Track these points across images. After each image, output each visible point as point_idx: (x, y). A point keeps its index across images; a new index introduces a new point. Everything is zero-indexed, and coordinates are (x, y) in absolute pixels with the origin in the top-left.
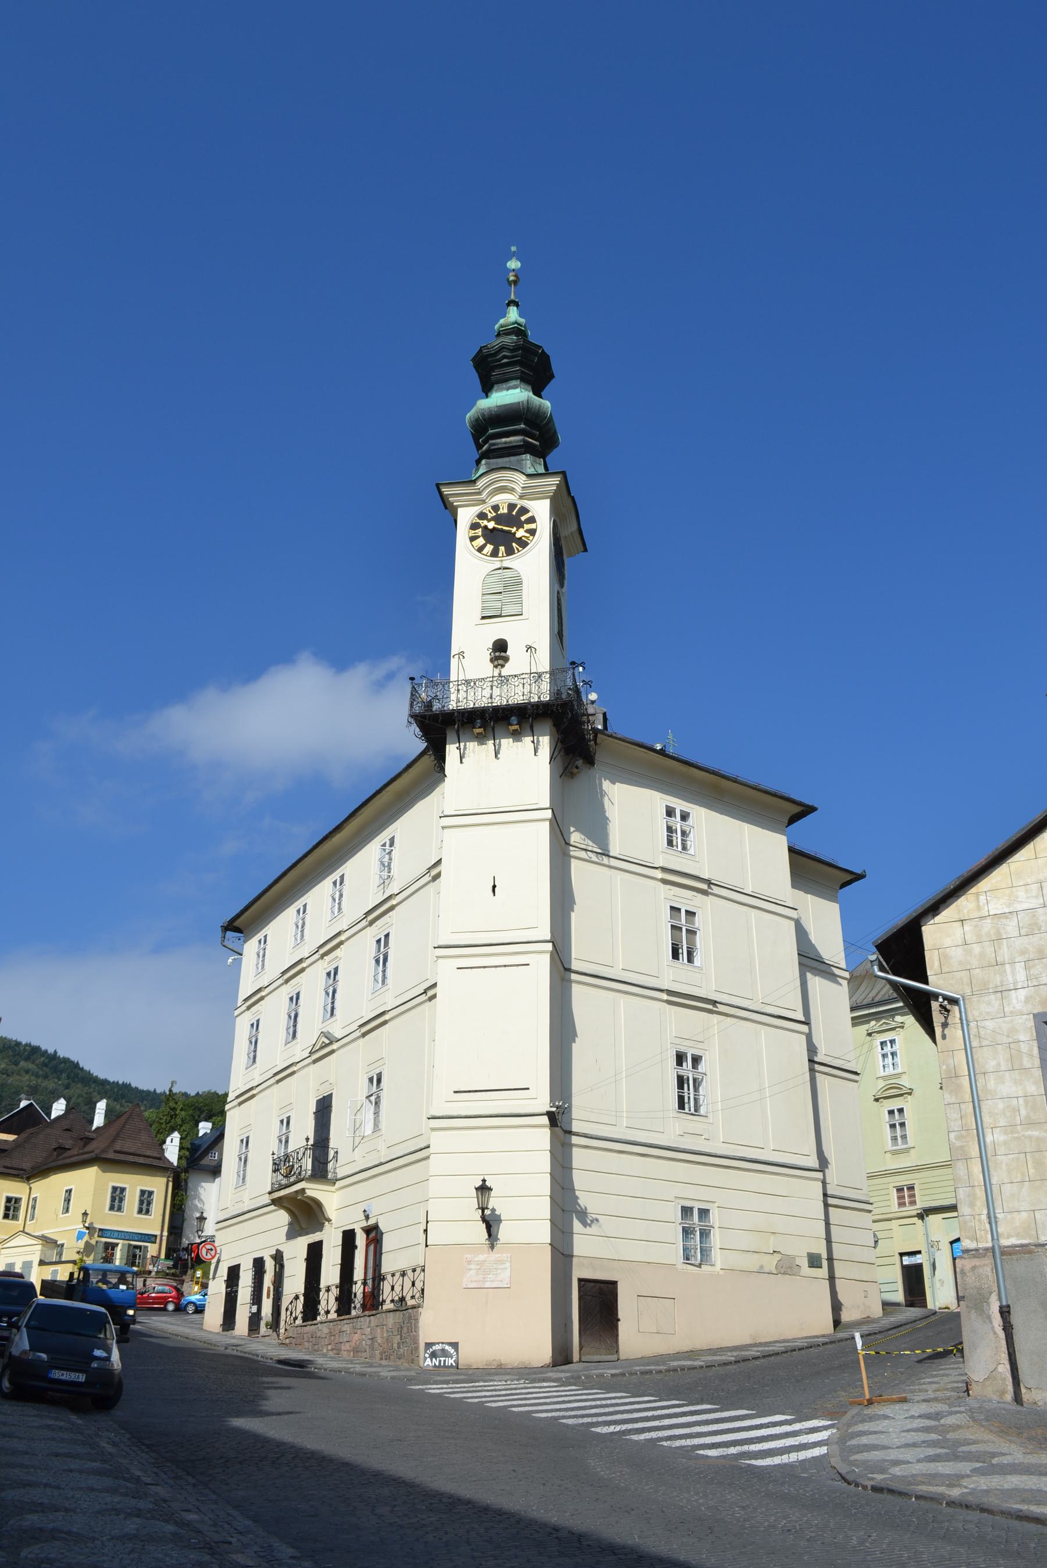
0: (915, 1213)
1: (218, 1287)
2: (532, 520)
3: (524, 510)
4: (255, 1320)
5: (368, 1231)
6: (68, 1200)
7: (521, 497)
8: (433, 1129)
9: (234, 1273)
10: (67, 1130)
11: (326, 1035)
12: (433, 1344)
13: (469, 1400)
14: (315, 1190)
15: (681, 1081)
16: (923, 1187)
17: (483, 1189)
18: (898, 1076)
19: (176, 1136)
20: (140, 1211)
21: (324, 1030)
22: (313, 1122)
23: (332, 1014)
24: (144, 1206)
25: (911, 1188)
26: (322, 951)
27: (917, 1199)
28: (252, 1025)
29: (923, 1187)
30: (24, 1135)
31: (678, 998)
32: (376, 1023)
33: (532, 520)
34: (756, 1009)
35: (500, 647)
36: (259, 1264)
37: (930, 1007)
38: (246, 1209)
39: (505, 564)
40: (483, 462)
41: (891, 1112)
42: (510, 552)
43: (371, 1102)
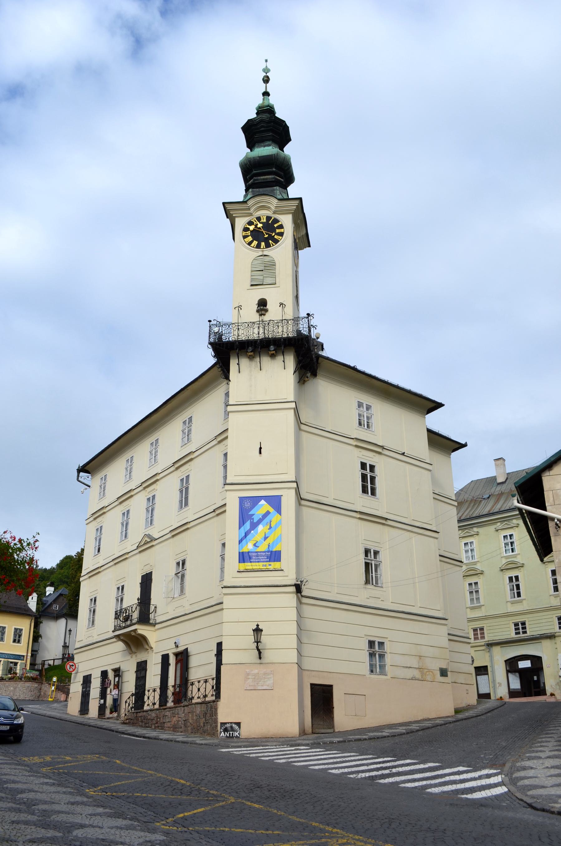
0: (483, 644)
1: (76, 688)
2: (281, 227)
3: (276, 221)
4: (102, 708)
5: (177, 655)
7: (274, 213)
8: (225, 594)
9: (87, 680)
11: (149, 536)
12: (226, 723)
13: (263, 758)
14: (142, 630)
15: (367, 565)
16: (489, 628)
18: (475, 563)
19: (35, 595)
20: (14, 641)
21: (147, 533)
22: (140, 589)
23: (151, 524)
24: (17, 638)
25: (482, 629)
26: (144, 485)
27: (486, 635)
28: (97, 530)
29: (489, 628)
31: (365, 517)
32: (182, 529)
34: (409, 523)
35: (262, 304)
36: (104, 674)
37: (548, 525)
38: (95, 641)
39: (265, 253)
40: (250, 190)
41: (470, 584)
42: (268, 246)
43: (178, 577)
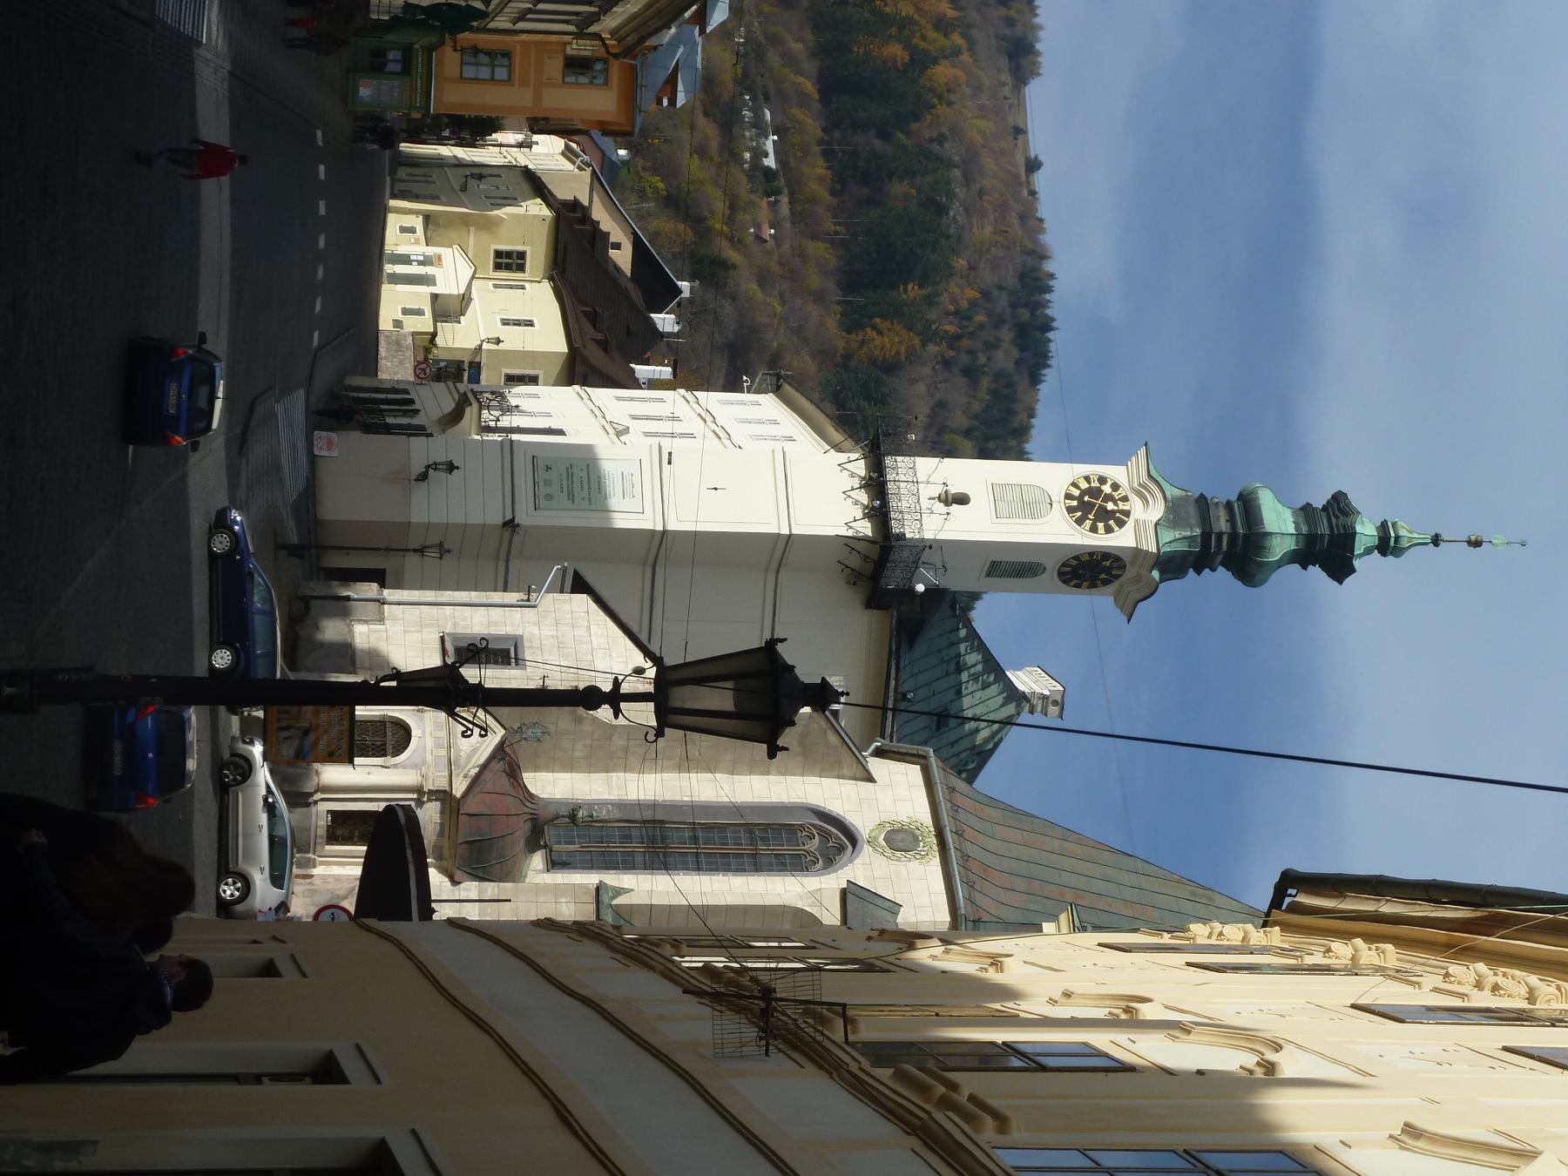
6: (518, 323)
10: (629, 330)
17: (451, 467)
30: (630, 286)
33: (1109, 530)
36: (412, 402)
